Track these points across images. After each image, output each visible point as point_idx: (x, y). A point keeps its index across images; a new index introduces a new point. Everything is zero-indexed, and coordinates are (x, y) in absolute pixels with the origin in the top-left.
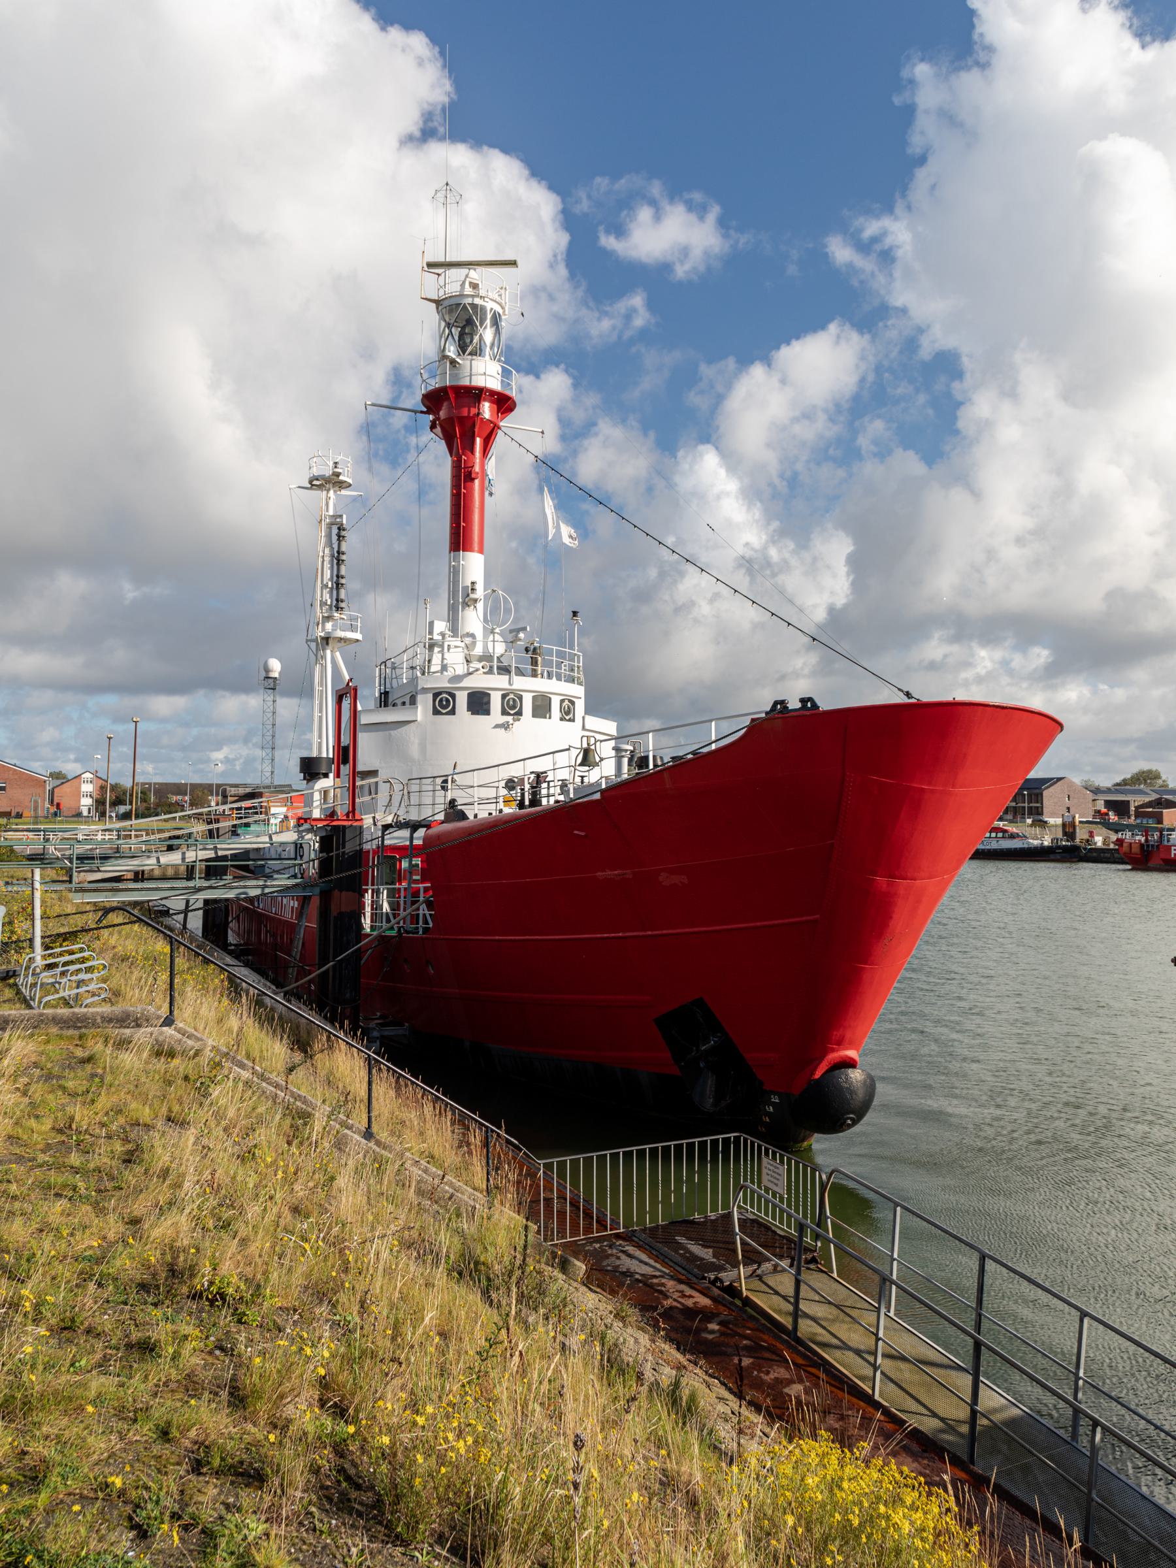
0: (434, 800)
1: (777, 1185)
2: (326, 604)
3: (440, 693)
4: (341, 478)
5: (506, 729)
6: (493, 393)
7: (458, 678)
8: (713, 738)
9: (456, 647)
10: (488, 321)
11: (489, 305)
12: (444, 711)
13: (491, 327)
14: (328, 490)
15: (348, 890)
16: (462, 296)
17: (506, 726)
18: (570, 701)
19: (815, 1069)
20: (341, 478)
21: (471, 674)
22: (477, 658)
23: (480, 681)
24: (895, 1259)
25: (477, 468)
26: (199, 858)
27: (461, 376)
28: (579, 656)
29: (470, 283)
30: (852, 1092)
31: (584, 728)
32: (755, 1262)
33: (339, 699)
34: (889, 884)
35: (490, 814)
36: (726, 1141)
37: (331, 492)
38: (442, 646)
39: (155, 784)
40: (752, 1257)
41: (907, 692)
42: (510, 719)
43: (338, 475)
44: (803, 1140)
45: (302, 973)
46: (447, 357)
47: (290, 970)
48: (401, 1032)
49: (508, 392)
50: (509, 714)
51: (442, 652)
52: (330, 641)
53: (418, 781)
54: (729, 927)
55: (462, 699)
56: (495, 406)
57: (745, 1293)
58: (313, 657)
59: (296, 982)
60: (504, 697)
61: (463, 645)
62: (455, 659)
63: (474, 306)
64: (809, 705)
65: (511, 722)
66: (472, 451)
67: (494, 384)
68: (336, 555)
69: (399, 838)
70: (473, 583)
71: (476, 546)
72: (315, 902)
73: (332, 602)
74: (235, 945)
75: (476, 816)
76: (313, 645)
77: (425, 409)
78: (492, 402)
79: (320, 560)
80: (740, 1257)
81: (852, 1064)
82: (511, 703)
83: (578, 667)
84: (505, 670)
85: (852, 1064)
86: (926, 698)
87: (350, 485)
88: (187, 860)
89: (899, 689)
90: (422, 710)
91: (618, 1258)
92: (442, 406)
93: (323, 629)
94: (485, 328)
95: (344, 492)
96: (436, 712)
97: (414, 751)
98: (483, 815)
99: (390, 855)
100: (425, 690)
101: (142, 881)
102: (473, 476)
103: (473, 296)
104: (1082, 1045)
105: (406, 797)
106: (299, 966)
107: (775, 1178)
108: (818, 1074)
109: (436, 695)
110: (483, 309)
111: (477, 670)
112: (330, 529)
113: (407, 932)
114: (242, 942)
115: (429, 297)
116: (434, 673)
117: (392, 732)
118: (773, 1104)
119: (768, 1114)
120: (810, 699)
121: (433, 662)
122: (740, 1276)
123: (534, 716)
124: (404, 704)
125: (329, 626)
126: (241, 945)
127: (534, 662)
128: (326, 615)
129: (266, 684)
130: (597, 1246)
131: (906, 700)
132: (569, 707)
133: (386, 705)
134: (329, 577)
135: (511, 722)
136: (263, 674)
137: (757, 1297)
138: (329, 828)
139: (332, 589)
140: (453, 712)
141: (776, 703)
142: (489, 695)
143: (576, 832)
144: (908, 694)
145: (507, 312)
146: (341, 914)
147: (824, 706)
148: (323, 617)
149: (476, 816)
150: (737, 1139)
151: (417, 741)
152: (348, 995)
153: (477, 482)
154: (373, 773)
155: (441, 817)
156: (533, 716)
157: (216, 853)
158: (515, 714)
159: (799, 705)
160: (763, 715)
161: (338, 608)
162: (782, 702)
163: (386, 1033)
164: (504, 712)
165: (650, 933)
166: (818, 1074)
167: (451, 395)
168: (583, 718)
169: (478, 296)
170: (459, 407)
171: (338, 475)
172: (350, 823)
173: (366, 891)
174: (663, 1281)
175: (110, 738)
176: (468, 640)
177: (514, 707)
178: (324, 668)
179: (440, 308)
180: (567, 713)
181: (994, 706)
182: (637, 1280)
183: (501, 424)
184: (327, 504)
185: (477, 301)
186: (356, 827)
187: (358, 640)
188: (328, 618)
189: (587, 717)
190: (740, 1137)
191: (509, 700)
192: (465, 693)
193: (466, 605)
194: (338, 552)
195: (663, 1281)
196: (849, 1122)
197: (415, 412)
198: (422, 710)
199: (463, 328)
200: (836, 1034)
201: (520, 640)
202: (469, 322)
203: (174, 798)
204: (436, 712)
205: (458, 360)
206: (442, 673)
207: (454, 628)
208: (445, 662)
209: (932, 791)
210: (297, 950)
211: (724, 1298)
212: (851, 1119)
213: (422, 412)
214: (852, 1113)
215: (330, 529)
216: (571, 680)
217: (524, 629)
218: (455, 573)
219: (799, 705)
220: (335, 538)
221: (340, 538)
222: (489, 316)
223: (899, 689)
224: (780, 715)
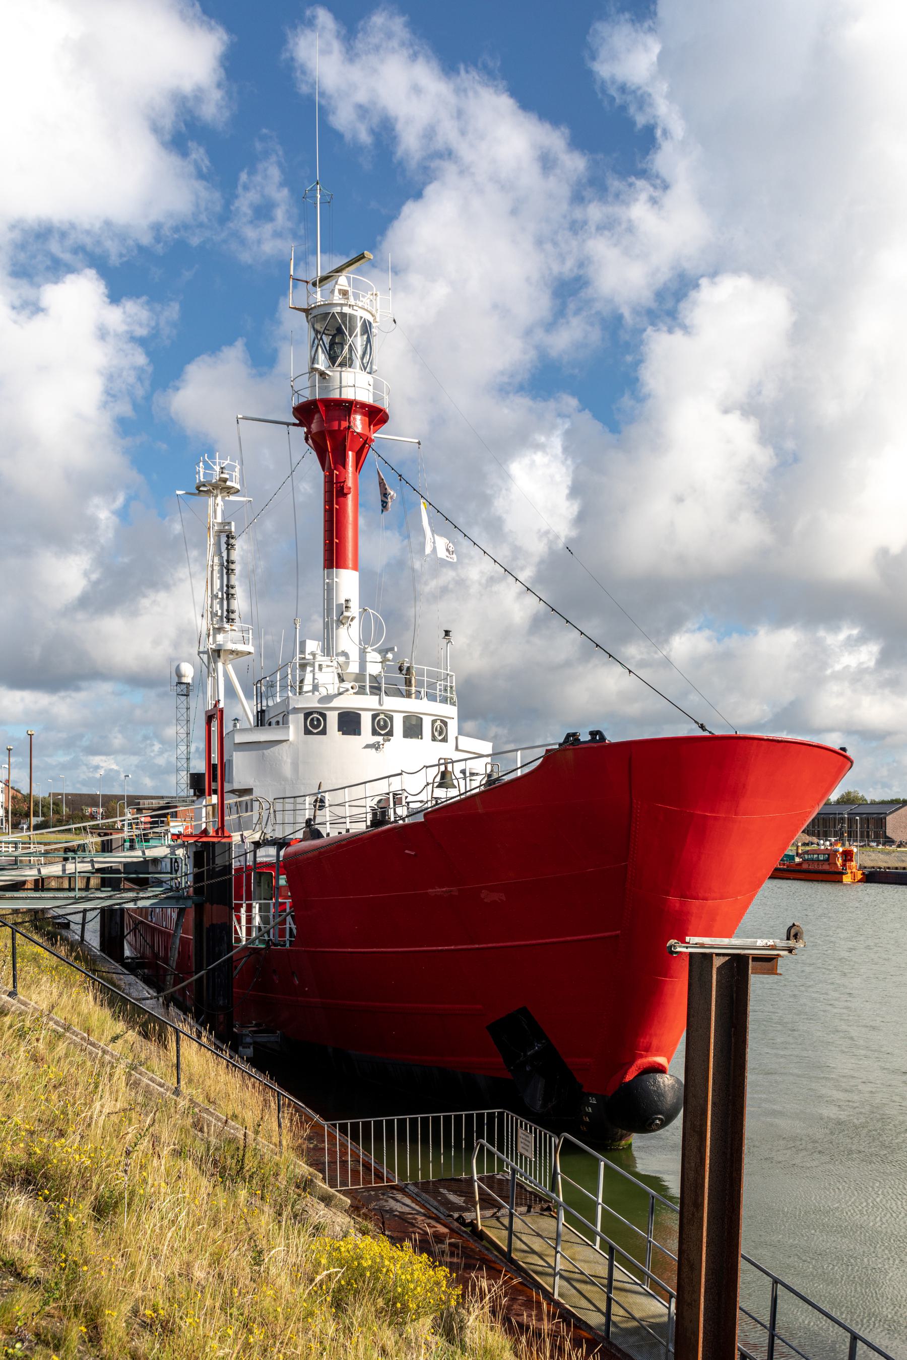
1: (527, 1150)
2: (216, 615)
3: (311, 713)
4: (228, 483)
5: (377, 749)
6: (363, 405)
7: (329, 698)
8: (519, 765)
9: (328, 666)
10: (358, 330)
11: (359, 313)
12: (315, 731)
13: (362, 335)
14: (216, 496)
15: (218, 904)
16: (332, 305)
17: (376, 747)
18: (442, 721)
19: (626, 1073)
20: (228, 483)
21: (340, 694)
22: (353, 677)
23: (350, 701)
24: (599, 1204)
25: (350, 483)
26: (78, 870)
27: (331, 388)
28: (452, 676)
29: (340, 290)
30: (661, 1095)
31: (457, 749)
32: (496, 1207)
33: (210, 718)
34: (683, 904)
35: (340, 833)
36: (491, 1116)
37: (219, 498)
38: (313, 665)
39: (67, 795)
40: (487, 1202)
41: (702, 725)
42: (380, 739)
43: (225, 481)
44: (621, 1139)
45: (178, 980)
46: (316, 369)
47: (168, 977)
48: (272, 1039)
49: (378, 404)
50: (380, 735)
51: (313, 671)
52: (222, 654)
53: (281, 800)
54: (544, 941)
55: (333, 719)
56: (367, 419)
57: (480, 1228)
58: (205, 669)
59: (174, 986)
60: (374, 717)
61: (335, 664)
62: (327, 680)
63: (343, 315)
65: (382, 742)
66: (344, 464)
67: (366, 397)
68: (225, 564)
69: (267, 854)
70: (347, 601)
71: (350, 563)
72: (191, 915)
73: (222, 613)
74: (132, 958)
75: (328, 835)
76: (205, 657)
77: (297, 422)
78: (364, 414)
79: (210, 569)
80: (477, 1199)
81: (661, 1070)
82: (382, 723)
83: (451, 687)
84: (376, 690)
85: (661, 1070)
86: (718, 732)
87: (238, 491)
88: (67, 872)
90: (294, 730)
91: (387, 1201)
92: (313, 419)
93: (215, 641)
94: (356, 336)
95: (232, 498)
96: (307, 732)
97: (287, 770)
98: (334, 834)
99: (262, 871)
100: (296, 710)
101: (42, 891)
102: (345, 491)
103: (342, 305)
105: (272, 815)
106: (175, 974)
107: (526, 1145)
108: (629, 1077)
109: (307, 715)
110: (352, 318)
111: (347, 690)
112: (219, 536)
113: (275, 945)
114: (139, 955)
116: (307, 692)
117: (265, 751)
118: (592, 1105)
119: (588, 1114)
120: (598, 732)
121: (306, 682)
122: (478, 1216)
123: (406, 735)
125: (220, 638)
126: (137, 958)
127: (408, 683)
128: (216, 626)
129: (179, 690)
130: (373, 1193)
131: (700, 733)
132: (441, 727)
134: (218, 587)
135: (382, 742)
136: (176, 680)
137: (490, 1231)
138: (199, 844)
139: (222, 599)
140: (323, 732)
141: (568, 736)
143: (407, 851)
144: (702, 727)
145: (378, 320)
146: (212, 925)
147: (612, 737)
148: (214, 628)
149: (348, 831)
150: (501, 1115)
151: (289, 761)
152: (221, 1003)
153: (350, 497)
154: (248, 791)
155: (300, 835)
156: (404, 737)
157: (93, 866)
158: (386, 734)
159: (589, 738)
160: (557, 747)
161: (230, 620)
162: (574, 735)
163: (259, 1040)
164: (375, 733)
165: (477, 946)
166: (629, 1077)
167: (322, 408)
168: (457, 738)
169: (346, 305)
170: (330, 420)
172: (219, 839)
173: (241, 905)
174: (416, 1216)
175: (9, 750)
176: (342, 659)
178: (216, 680)
179: (310, 317)
180: (440, 733)
181: (768, 740)
182: (396, 1216)
183: (374, 436)
184: (215, 512)
185: (346, 310)
186: (225, 843)
187: (250, 653)
188: (220, 630)
189: (460, 737)
190: (504, 1112)
191: (379, 721)
192: (336, 713)
193: (340, 622)
194: (228, 561)
195: (416, 1216)
196: (658, 1122)
197: (288, 424)
198: (294, 730)
199: (334, 336)
200: (643, 1041)
201: (389, 660)
202: (340, 331)
203: (88, 811)
204: (307, 732)
205: (327, 372)
206: (313, 694)
207: (328, 649)
208: (316, 681)
209: (716, 818)
210: (174, 956)
211: (460, 1229)
212: (660, 1119)
213: (294, 425)
214: (661, 1114)
215: (219, 536)
216: (444, 700)
217: (392, 649)
218: (329, 590)
219: (589, 738)
220: (224, 546)
221: (230, 547)
222: (359, 324)
224: (571, 747)
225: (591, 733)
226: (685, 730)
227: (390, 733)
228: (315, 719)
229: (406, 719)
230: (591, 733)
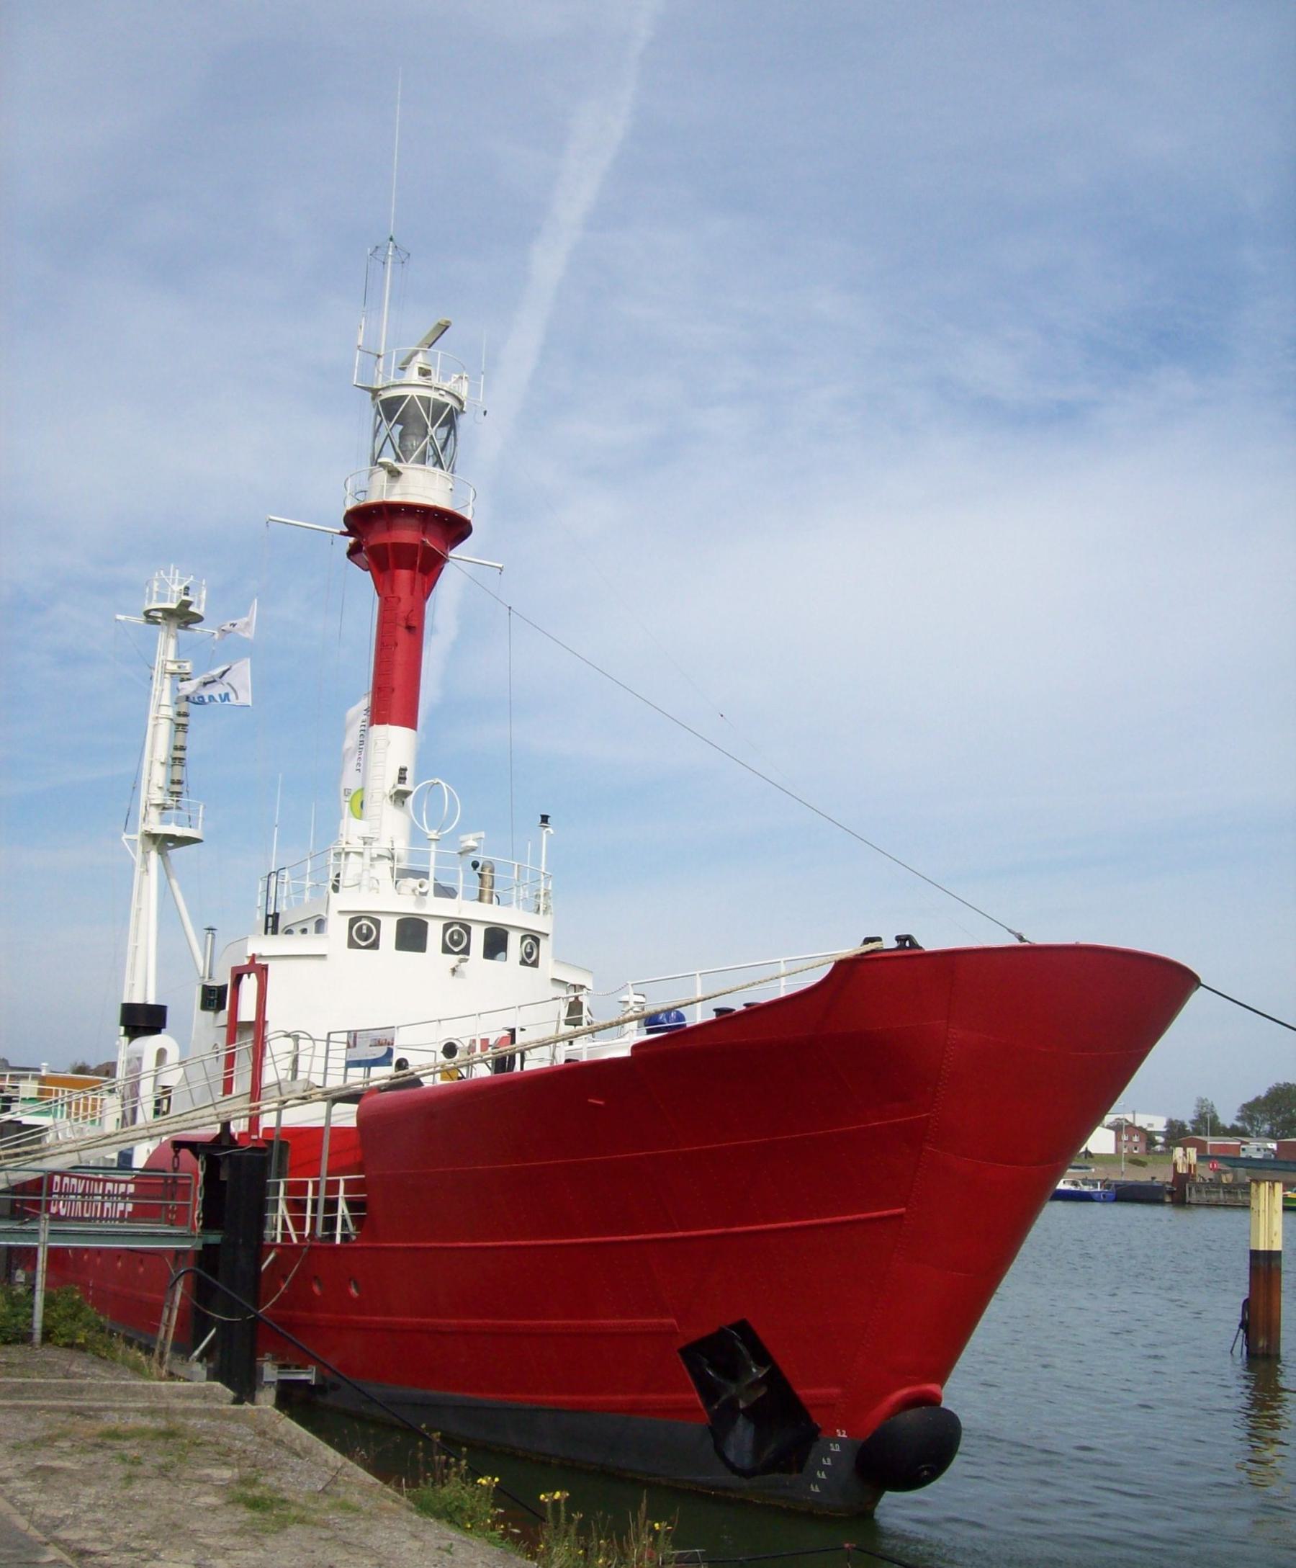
0: (313, 1052)
3: (359, 919)
18: (463, 926)
43: (188, 604)
64: (907, 944)
77: (346, 530)
89: (1010, 931)
104: (1116, 1291)
115: (228, 673)
118: (841, 1441)
120: (909, 938)
124: (304, 931)
131: (1016, 943)
133: (275, 932)
140: (375, 945)
142: (426, 924)
143: (601, 1103)
144: (1021, 939)
159: (894, 944)
171: (188, 604)
177: (457, 944)
219: (894, 944)
223: (1010, 931)
225: (898, 938)
226: (1006, 940)
227: (466, 951)
228: (364, 927)
229: (401, 924)
230: (898, 938)
